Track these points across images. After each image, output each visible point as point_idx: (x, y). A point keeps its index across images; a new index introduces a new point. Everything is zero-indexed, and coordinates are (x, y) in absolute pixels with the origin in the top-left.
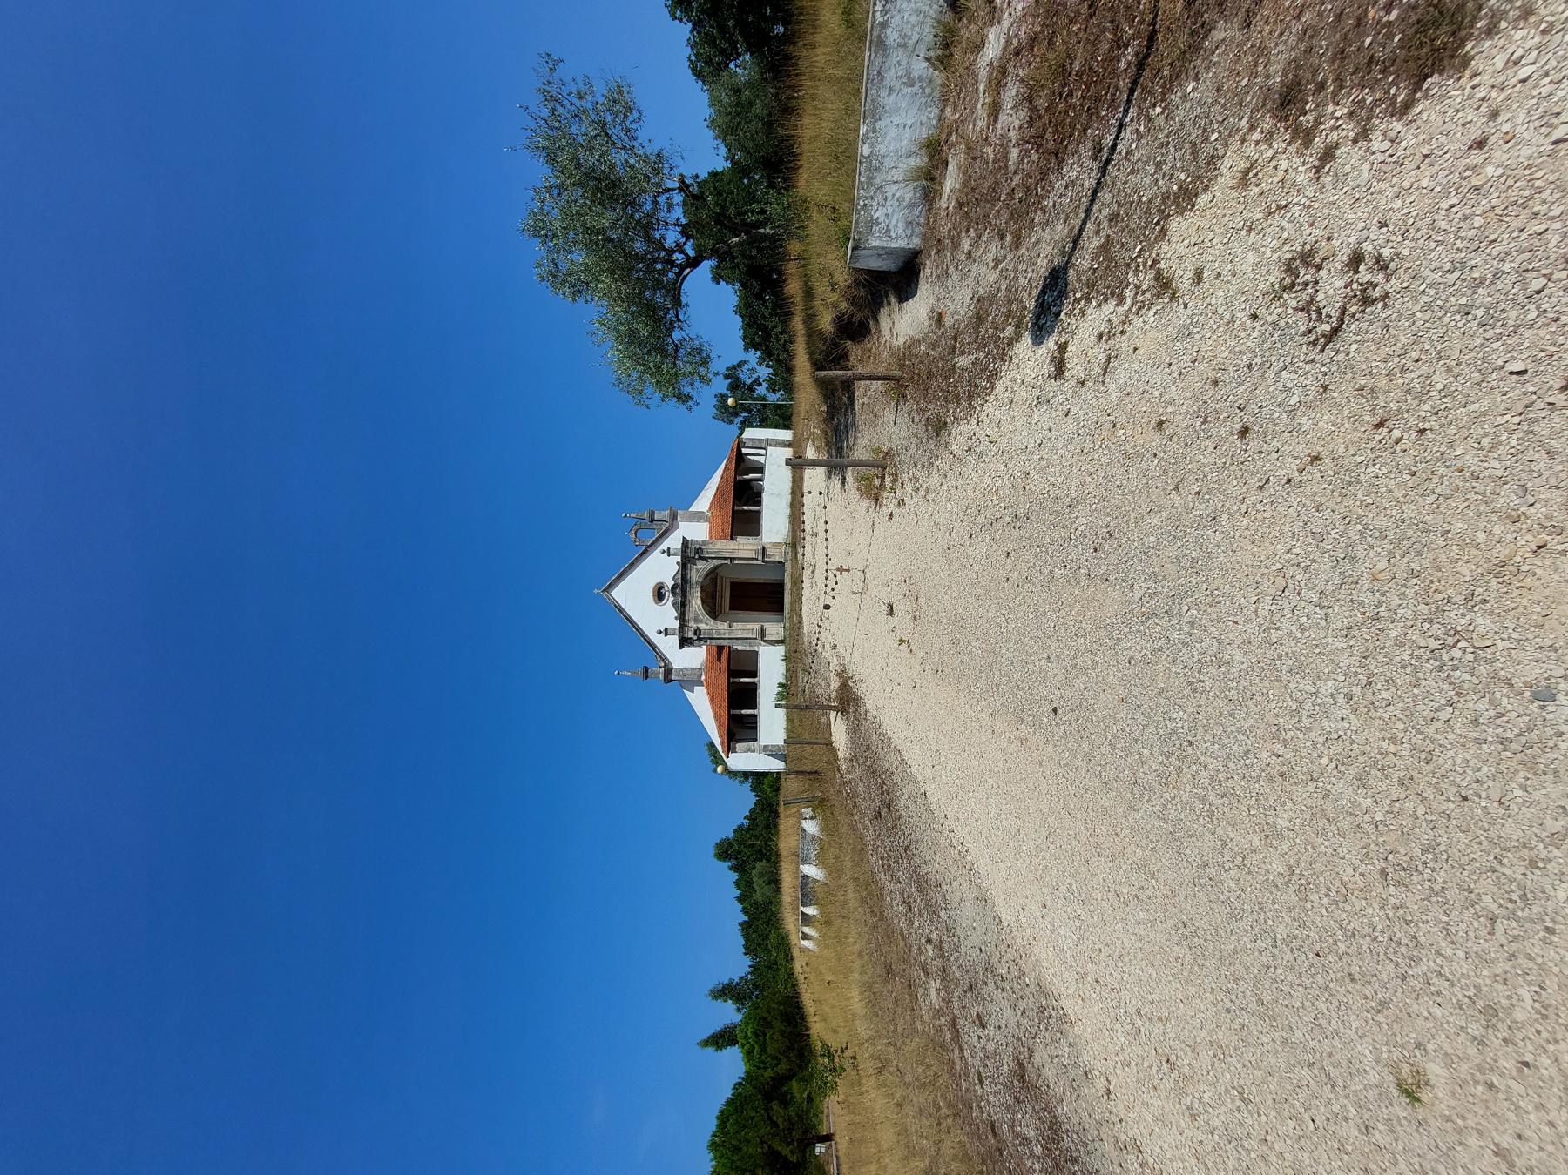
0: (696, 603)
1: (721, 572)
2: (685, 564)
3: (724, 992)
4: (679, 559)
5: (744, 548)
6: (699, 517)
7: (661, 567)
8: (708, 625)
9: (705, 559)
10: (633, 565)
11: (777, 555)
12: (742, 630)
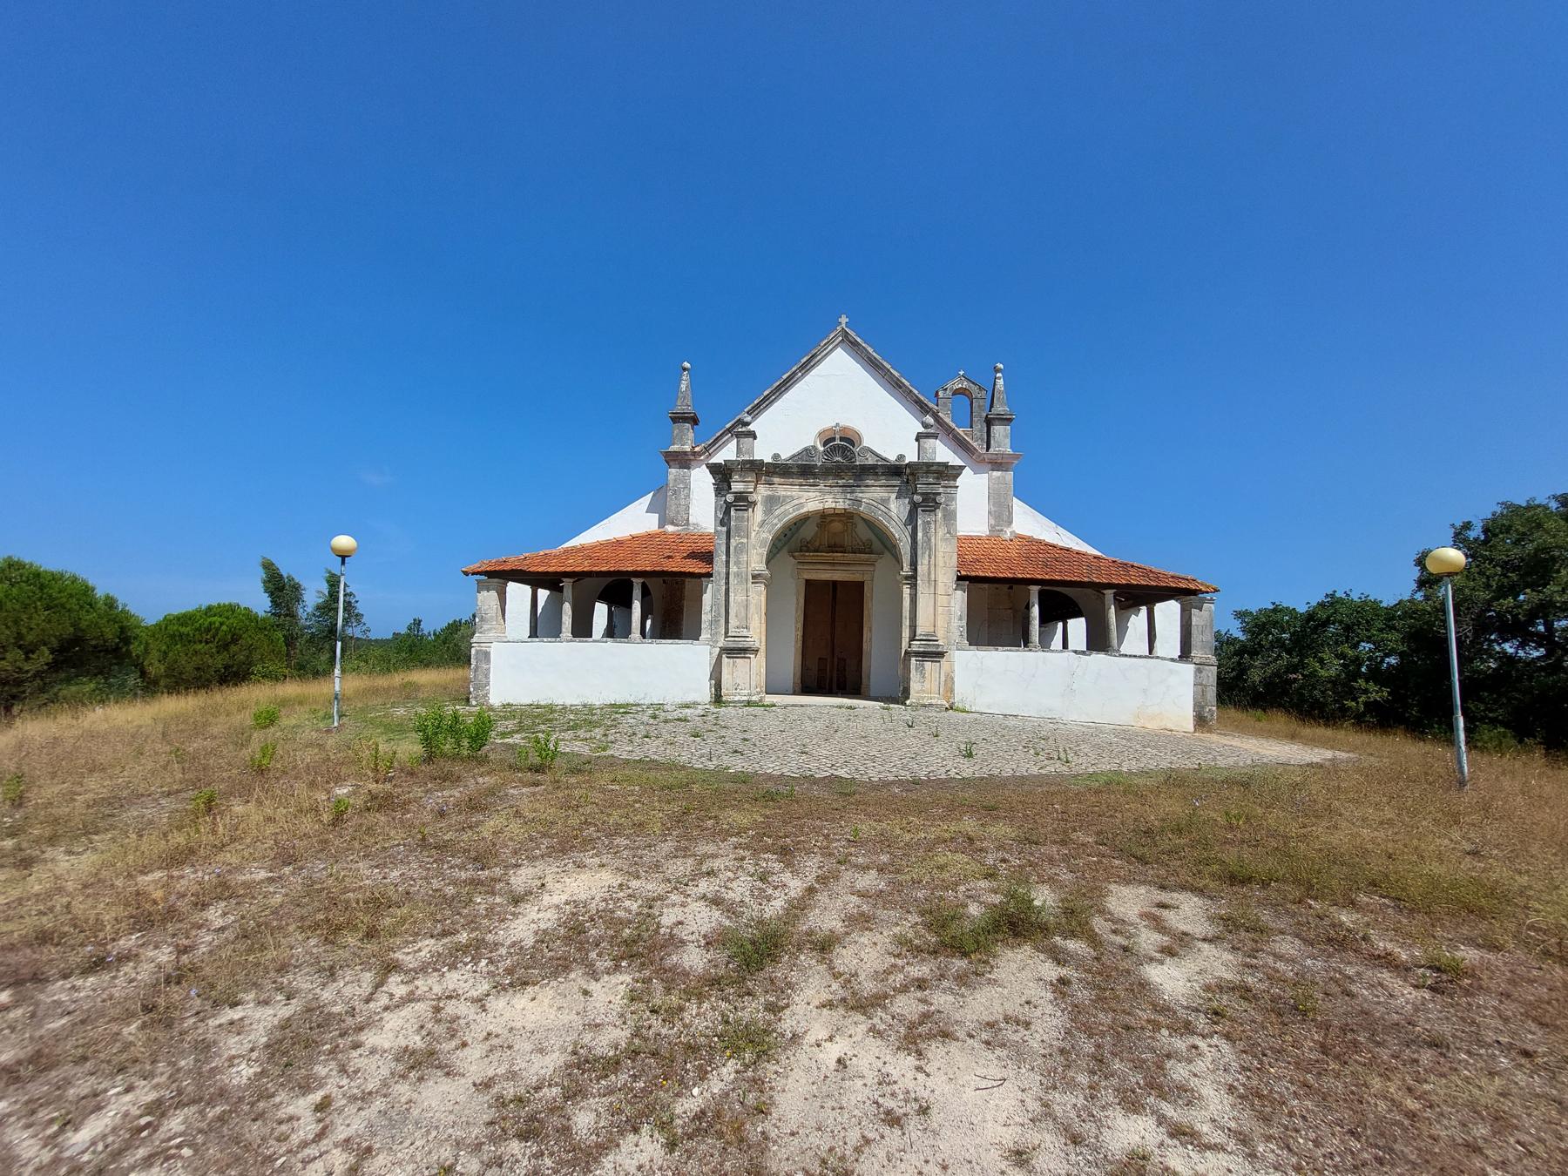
0: (812, 499)
1: (883, 563)
2: (896, 472)
3: (1240, 615)
4: (911, 457)
5: (940, 607)
6: (1001, 514)
7: (891, 431)
8: (759, 528)
9: (912, 519)
10: (895, 386)
11: (924, 683)
12: (748, 604)
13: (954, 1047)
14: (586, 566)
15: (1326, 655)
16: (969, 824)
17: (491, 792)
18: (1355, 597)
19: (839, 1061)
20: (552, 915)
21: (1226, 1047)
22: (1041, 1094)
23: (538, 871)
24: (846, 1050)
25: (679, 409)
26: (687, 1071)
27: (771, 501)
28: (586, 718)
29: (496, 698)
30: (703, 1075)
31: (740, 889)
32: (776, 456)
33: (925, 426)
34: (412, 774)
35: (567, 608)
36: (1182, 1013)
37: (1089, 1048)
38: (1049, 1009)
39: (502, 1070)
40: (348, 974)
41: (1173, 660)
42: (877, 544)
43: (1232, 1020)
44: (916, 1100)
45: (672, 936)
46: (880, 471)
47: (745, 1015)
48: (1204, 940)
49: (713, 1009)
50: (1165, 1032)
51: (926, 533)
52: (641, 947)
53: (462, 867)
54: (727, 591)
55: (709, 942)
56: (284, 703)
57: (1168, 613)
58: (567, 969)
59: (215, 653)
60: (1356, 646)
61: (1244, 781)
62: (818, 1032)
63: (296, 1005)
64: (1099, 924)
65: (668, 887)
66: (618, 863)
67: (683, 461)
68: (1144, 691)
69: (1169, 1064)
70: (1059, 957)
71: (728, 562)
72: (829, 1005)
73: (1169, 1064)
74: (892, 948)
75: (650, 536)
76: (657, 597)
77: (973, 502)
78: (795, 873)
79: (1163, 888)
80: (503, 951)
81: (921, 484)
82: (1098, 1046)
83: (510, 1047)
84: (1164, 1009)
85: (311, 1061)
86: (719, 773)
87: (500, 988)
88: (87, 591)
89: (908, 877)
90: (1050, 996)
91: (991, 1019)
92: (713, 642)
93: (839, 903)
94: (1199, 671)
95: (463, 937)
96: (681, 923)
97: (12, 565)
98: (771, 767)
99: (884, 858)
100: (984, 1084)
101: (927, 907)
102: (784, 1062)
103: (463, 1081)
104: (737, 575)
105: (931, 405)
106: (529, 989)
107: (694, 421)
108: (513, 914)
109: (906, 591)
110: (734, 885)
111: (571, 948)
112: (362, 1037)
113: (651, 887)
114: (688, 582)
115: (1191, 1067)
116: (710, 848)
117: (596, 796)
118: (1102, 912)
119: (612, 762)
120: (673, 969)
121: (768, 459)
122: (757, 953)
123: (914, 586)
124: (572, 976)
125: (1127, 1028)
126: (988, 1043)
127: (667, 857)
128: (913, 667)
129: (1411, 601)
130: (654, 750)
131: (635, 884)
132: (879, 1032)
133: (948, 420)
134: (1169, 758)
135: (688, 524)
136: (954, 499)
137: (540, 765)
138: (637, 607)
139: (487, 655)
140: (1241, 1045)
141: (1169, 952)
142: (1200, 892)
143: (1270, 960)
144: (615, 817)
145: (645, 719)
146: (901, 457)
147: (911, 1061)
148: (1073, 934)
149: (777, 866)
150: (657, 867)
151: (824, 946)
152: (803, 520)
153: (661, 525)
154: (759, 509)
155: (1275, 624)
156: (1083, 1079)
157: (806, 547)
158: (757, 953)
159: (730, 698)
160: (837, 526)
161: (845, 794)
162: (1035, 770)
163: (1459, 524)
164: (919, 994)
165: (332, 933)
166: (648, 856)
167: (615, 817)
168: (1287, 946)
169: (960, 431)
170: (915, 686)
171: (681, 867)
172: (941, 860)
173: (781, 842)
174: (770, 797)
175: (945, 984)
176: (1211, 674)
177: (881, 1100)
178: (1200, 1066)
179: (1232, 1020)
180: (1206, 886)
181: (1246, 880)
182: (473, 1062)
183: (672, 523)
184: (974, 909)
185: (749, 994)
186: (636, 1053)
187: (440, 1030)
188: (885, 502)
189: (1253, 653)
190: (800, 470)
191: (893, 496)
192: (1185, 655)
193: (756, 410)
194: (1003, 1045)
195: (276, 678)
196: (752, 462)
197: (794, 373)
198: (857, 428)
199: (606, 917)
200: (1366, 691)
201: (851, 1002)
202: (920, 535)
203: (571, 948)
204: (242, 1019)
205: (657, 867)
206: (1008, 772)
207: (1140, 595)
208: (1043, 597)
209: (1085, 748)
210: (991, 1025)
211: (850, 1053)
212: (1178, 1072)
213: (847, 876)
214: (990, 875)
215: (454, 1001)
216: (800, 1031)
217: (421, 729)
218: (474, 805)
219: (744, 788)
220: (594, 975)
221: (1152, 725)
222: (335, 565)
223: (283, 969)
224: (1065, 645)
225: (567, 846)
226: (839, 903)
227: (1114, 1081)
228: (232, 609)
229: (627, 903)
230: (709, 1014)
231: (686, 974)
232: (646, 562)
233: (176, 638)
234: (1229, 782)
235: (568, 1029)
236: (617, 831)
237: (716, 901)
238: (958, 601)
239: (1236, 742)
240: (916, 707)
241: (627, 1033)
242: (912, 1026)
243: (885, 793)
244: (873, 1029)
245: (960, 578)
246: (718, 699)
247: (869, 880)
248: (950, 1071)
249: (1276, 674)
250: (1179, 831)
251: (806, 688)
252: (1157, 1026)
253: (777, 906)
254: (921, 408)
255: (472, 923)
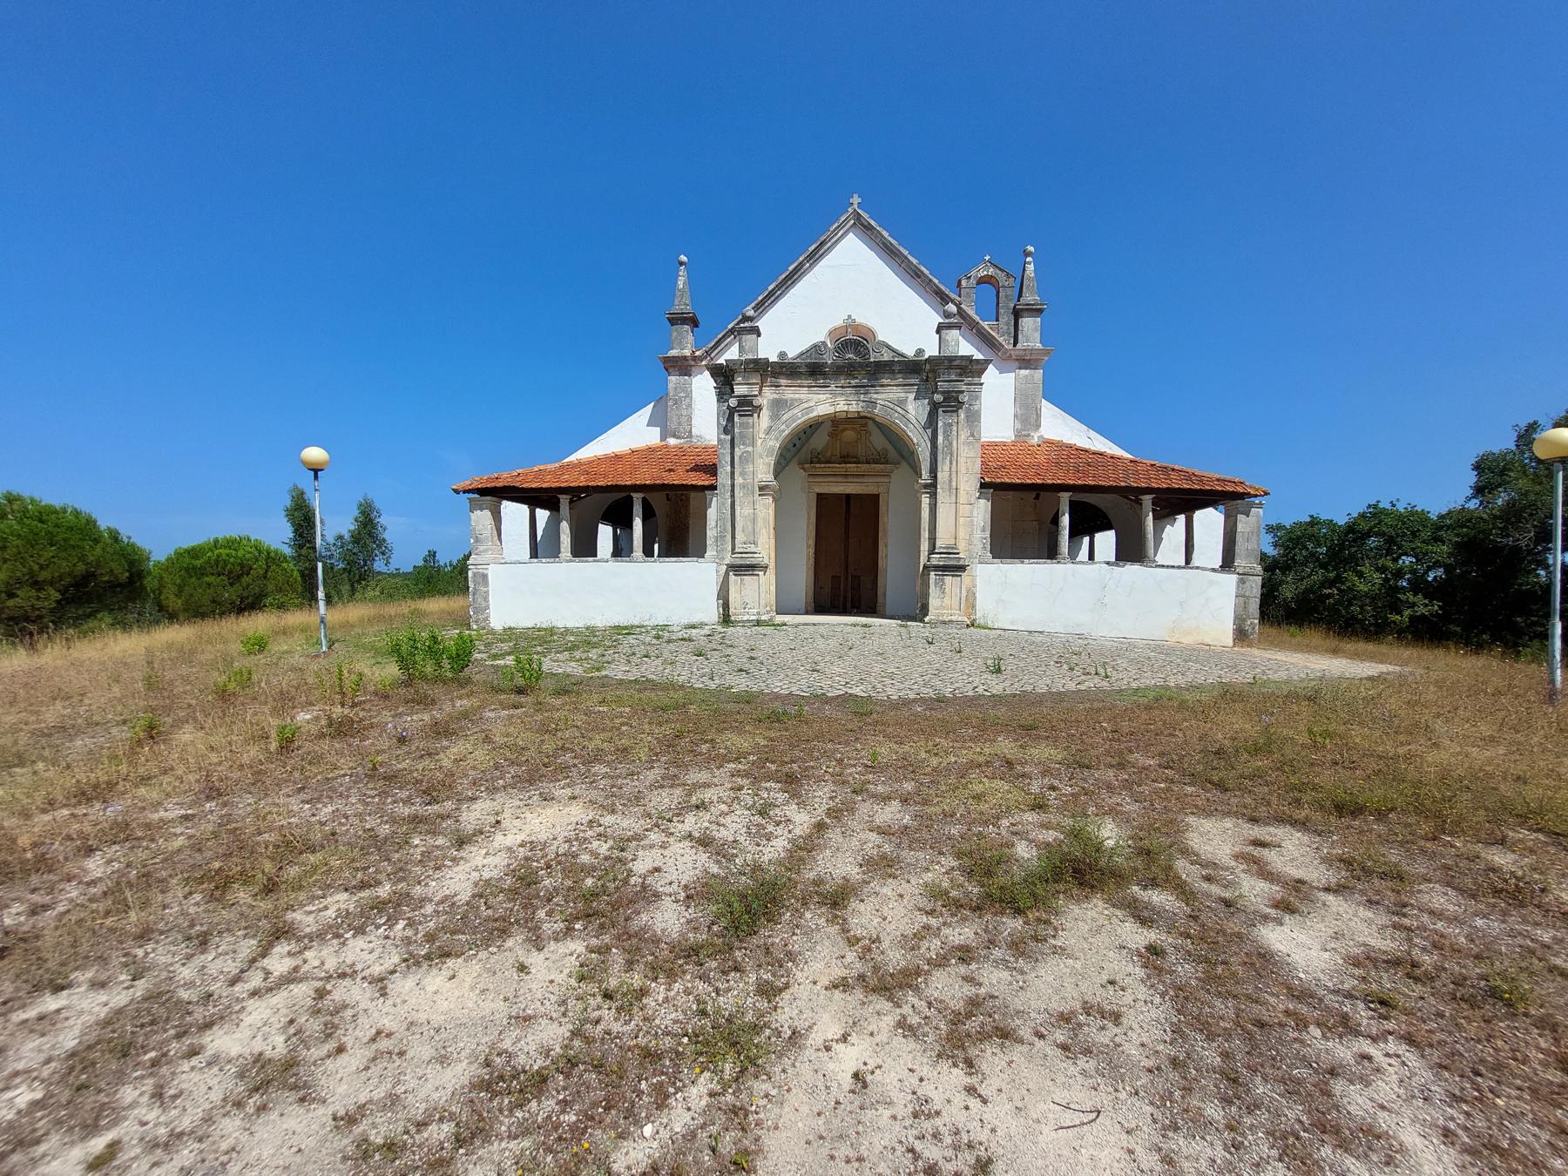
0: (822, 402)
1: (900, 474)
3: (1270, 529)
4: (932, 350)
5: (962, 517)
6: (1028, 417)
7: (908, 324)
8: (766, 436)
11: (943, 599)
12: (754, 517)
13: (1017, 1053)
14: (582, 481)
15: (1366, 568)
16: (1006, 746)
17: (465, 715)
18: (1401, 508)
19: (856, 1076)
20: (501, 860)
21: (1412, 1058)
22: (1157, 1139)
23: (496, 806)
24: (865, 1057)
25: (676, 309)
26: (640, 1093)
27: (779, 406)
28: (588, 639)
29: (497, 621)
30: (662, 1100)
31: (734, 826)
32: (782, 355)
33: (947, 315)
34: (386, 697)
35: (565, 527)
36: (1331, 1000)
37: (1211, 1055)
38: (1143, 992)
39: (379, 1093)
40: (225, 943)
41: (1214, 570)
42: (893, 454)
43: (1408, 1012)
44: (970, 1146)
45: (644, 887)
46: (897, 368)
47: (727, 1003)
48: (1327, 890)
49: (687, 992)
50: (1315, 1032)
51: (947, 437)
52: (599, 901)
53: (408, 801)
54: (733, 504)
55: (691, 896)
56: (285, 632)
57: (1209, 521)
58: (504, 933)
59: (228, 583)
60: (1395, 560)
61: (1312, 696)
62: (828, 1028)
63: (142, 986)
64: (1182, 866)
65: (648, 823)
66: (593, 794)
67: (683, 367)
68: (1181, 604)
69: (1338, 1086)
70: (1143, 916)
71: (733, 473)
72: (841, 985)
73: (1338, 1086)
74: (924, 903)
75: (651, 450)
76: (663, 513)
77: (998, 402)
78: (802, 804)
79: (1254, 820)
80: (429, 909)
81: (944, 383)
82: (1226, 1055)
83: (401, 1054)
84: (1303, 994)
85: (120, 1078)
86: (722, 693)
87: (412, 962)
88: (91, 523)
89: (938, 810)
90: (1140, 972)
91: (1065, 1008)
92: (719, 560)
93: (855, 843)
94: (1241, 582)
95: (384, 891)
96: (657, 870)
97: (11, 499)
98: (779, 686)
99: (909, 786)
100: (1069, 1118)
101: (965, 846)
102: (778, 1077)
103: (321, 1111)
104: (743, 486)
105: (953, 296)
106: (450, 963)
107: (694, 322)
108: (454, 860)
109: (925, 500)
110: (728, 820)
111: (519, 904)
112: (206, 1038)
113: (626, 823)
114: (693, 495)
115: (1370, 1091)
116: (703, 776)
117: (580, 719)
118: (1185, 852)
119: (605, 683)
120: (639, 934)
121: (773, 358)
122: (749, 911)
123: (933, 495)
124: (510, 943)
125: (1261, 1025)
126: (1065, 1048)
127: (652, 787)
128: (932, 581)
129: (1463, 509)
130: (652, 670)
131: (608, 820)
132: (911, 1028)
133: (971, 313)
134: (1217, 672)
135: (690, 436)
136: (978, 398)
137: (524, 686)
138: (638, 524)
139: (485, 577)
140: (1436, 1055)
141: (1286, 907)
142: (1302, 825)
143: (1425, 918)
144: (597, 741)
145: (648, 639)
146: (920, 352)
147: (958, 1076)
148: (1153, 883)
149: (781, 797)
150: (638, 798)
151: (837, 899)
152: (813, 427)
153: (663, 438)
154: (765, 414)
155: (1312, 537)
156: (1214, 1111)
157: (816, 458)
158: (749, 911)
159: (739, 618)
160: (849, 435)
161: (861, 714)
162: (1072, 686)
163: (1523, 424)
164: (962, 969)
165: (219, 886)
166: (630, 786)
167: (597, 741)
168: (1440, 898)
169: (985, 324)
170: (934, 602)
171: (665, 799)
172: (979, 788)
173: (786, 769)
174: (775, 718)
175: (997, 953)
176: (1255, 586)
177: (918, 1146)
178: (1387, 1088)
179: (1408, 1012)
180: (1307, 818)
181: (1357, 811)
182: (344, 1081)
183: (674, 436)
184: (1023, 850)
185: (736, 969)
186: (572, 1063)
187: (314, 1026)
188: (901, 403)
189: (1286, 568)
190: (810, 369)
191: (912, 396)
192: (1228, 563)
193: (762, 307)
194: (1087, 1052)
195: (281, 607)
196: (756, 362)
197: (801, 264)
198: (871, 325)
199: (568, 865)
200: (1413, 605)
201: (873, 982)
202: (940, 438)
203: (519, 904)
204: (58, 1011)
205: (638, 798)
206: (1042, 689)
207: (1181, 501)
208: (1075, 508)
209: (1122, 663)
210: (1065, 1018)
211: (872, 1065)
212: (1356, 1101)
213: (864, 808)
214: (1039, 806)
215: (347, 982)
216: (800, 1025)
217: (396, 650)
218: (441, 731)
219: (747, 708)
220: (537, 943)
221: (1188, 640)
222: (305, 481)
223: (144, 935)
224: (1091, 556)
225: (534, 775)
226: (855, 843)
227: (1263, 1116)
228: (232, 544)
229: (595, 844)
230: (681, 1000)
231: (656, 941)
232: (645, 477)
233: (191, 571)
234: (1293, 696)
235: (487, 1023)
236: (597, 757)
237: (704, 842)
238: (982, 510)
239: (1267, 654)
240: (933, 624)
241: (564, 1031)
242: (957, 1019)
243: (905, 712)
244: (902, 1024)
245: (983, 486)
246: (726, 619)
247: (890, 813)
248: (1016, 1097)
249: (1309, 591)
250: (1256, 750)
251: (819, 608)
252: (1302, 1024)
253: (777, 848)
254: (944, 299)
255: (400, 873)
